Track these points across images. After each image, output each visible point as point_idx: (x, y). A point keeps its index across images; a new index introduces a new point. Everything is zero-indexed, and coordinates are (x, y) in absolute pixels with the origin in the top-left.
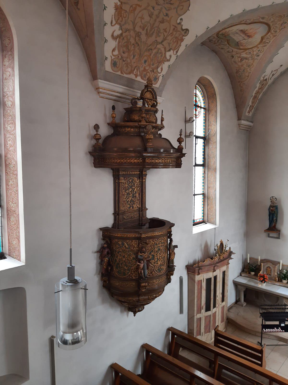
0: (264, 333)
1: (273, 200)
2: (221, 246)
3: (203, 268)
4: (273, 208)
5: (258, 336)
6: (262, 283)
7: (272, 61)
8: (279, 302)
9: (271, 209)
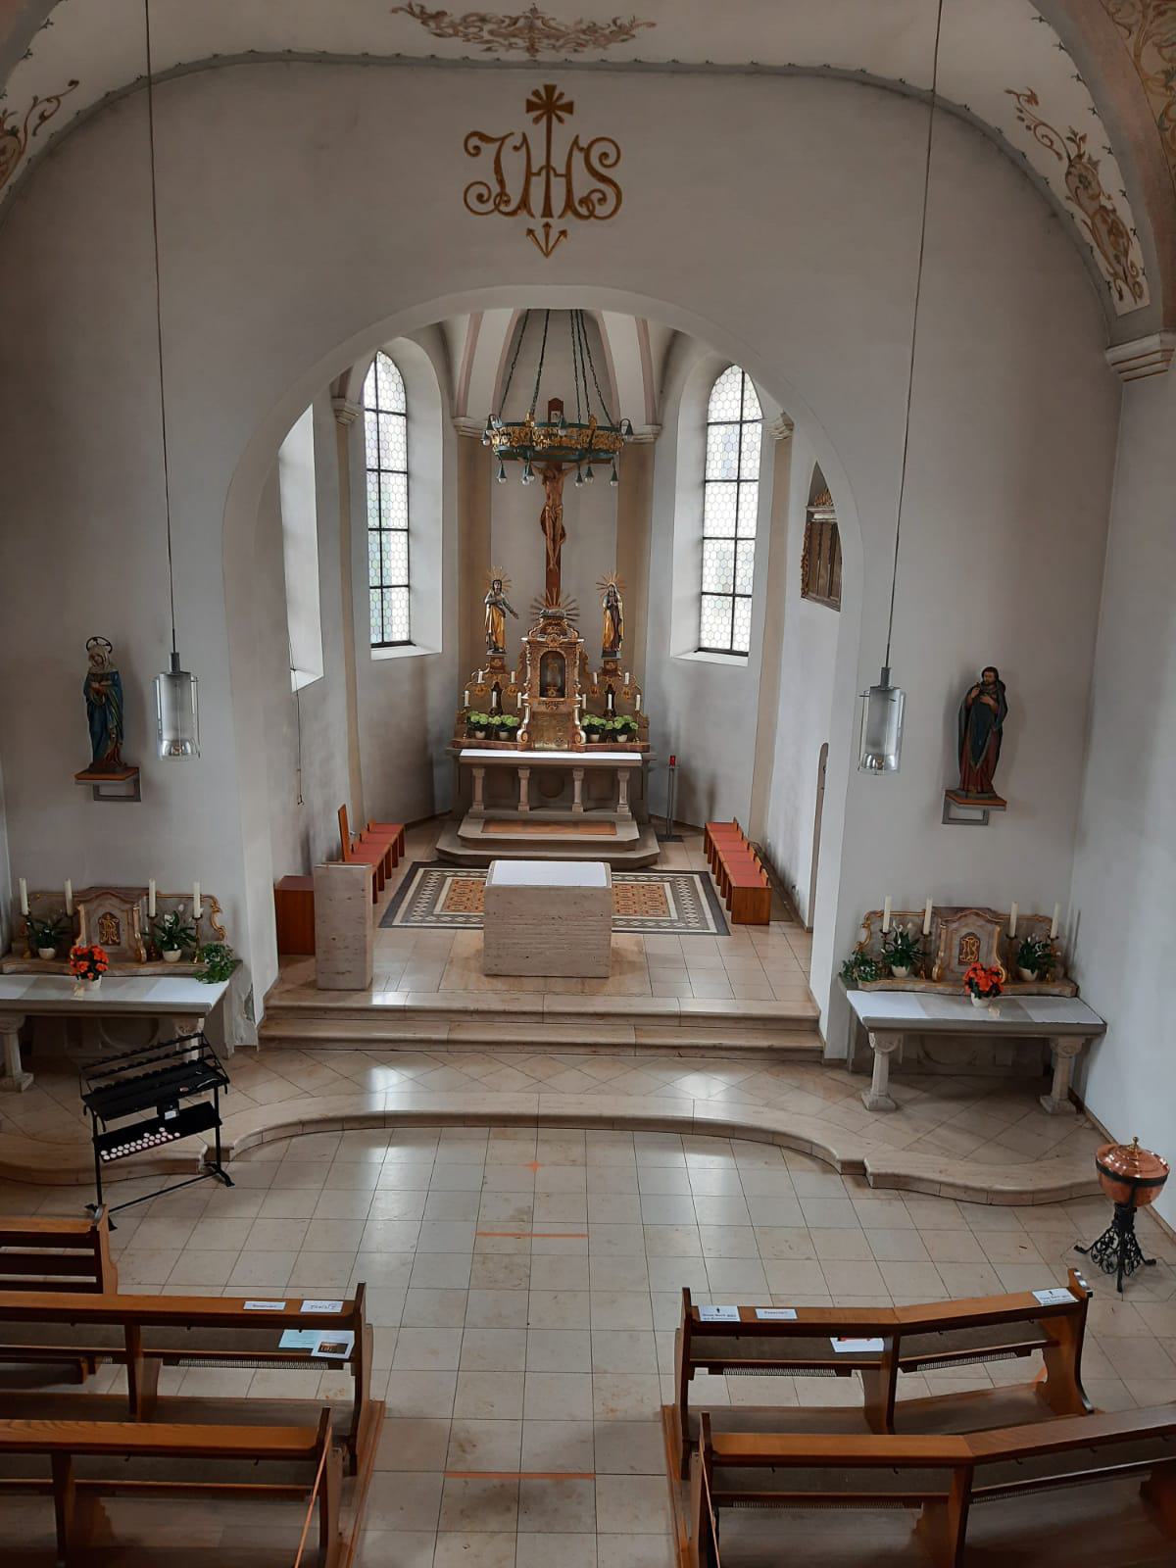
0: (106, 1164)
1: (96, 650)
7: (29, 53)
8: (161, 1036)
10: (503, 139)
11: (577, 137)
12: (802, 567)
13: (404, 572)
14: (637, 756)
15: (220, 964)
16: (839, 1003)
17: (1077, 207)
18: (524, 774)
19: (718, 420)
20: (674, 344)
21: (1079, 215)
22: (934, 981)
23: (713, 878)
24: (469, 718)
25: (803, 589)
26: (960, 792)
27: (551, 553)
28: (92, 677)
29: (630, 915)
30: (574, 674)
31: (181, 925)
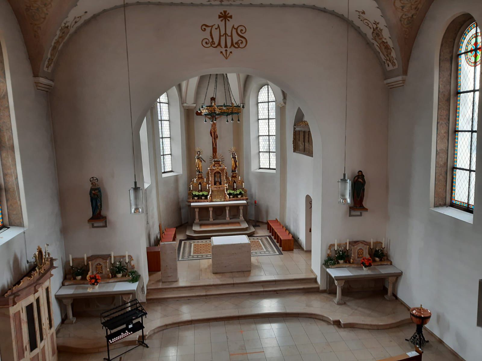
1: (94, 181)
2: (40, 255)
3: (19, 293)
4: (96, 191)
5: (96, 353)
6: (93, 286)
9: (93, 193)
10: (212, 26)
11: (234, 25)
12: (293, 143)
13: (169, 150)
14: (245, 202)
15: (135, 278)
16: (323, 272)
17: (375, 41)
18: (211, 210)
19: (261, 102)
20: (247, 80)
21: (376, 43)
22: (351, 264)
23: (273, 237)
24: (192, 193)
25: (294, 150)
26: (354, 207)
27: (214, 142)
28: (92, 189)
29: (207, 253)
30: (224, 178)
31: (122, 265)
